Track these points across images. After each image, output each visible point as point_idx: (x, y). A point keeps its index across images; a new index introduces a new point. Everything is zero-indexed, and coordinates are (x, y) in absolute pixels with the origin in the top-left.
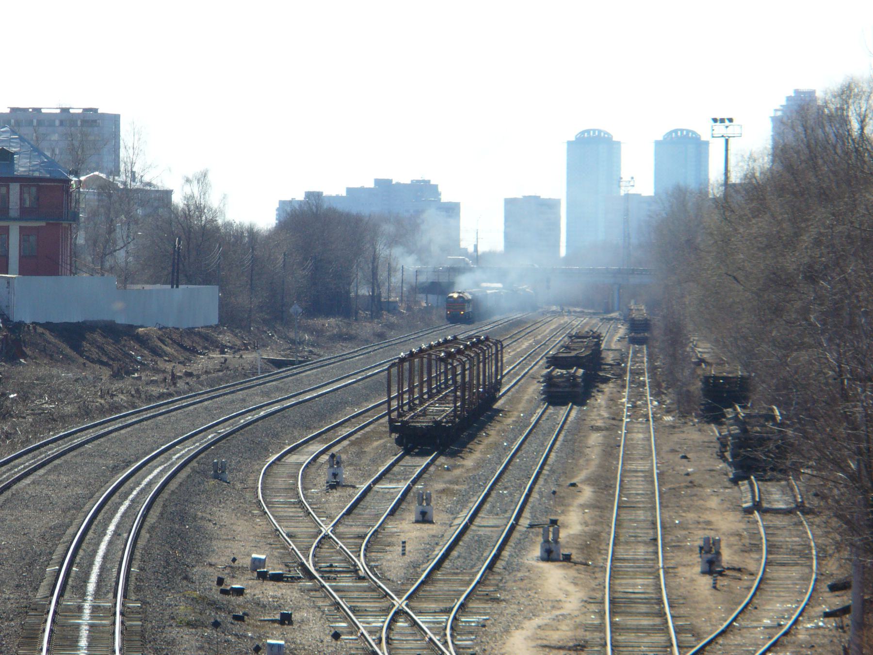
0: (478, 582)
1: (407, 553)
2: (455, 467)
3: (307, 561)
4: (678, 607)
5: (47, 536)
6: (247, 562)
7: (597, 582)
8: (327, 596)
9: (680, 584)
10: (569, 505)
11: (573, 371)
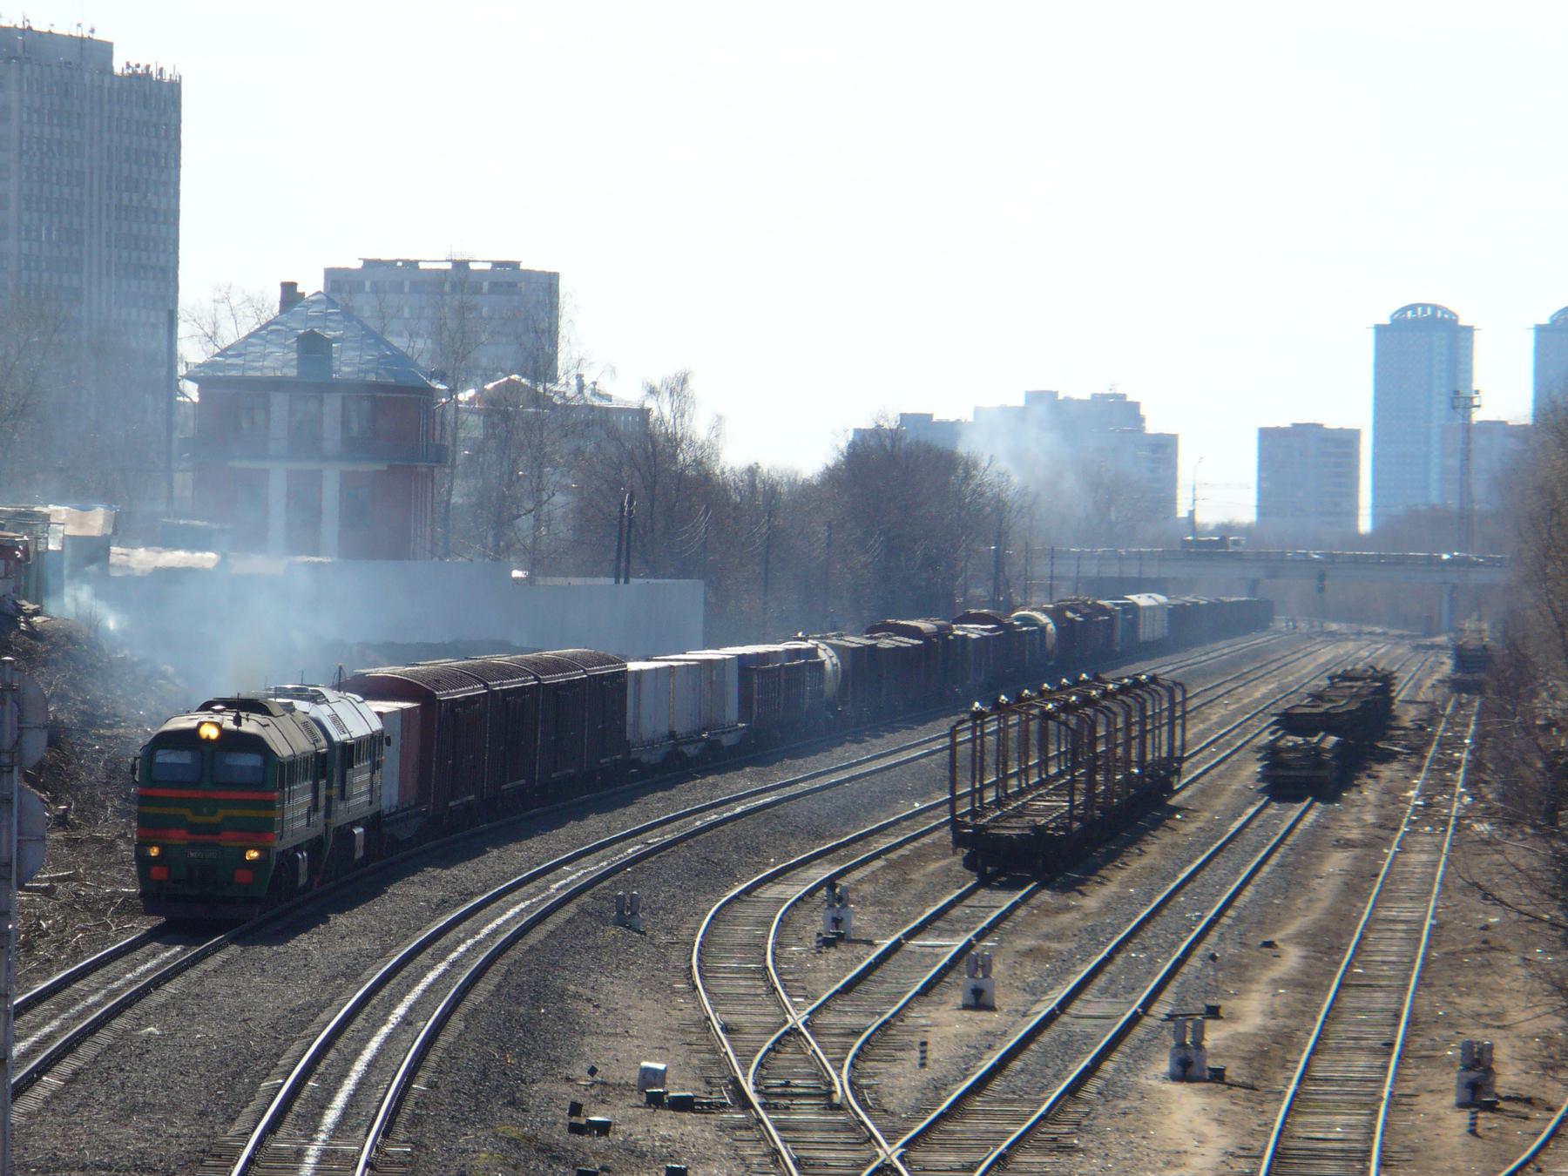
0: (1042, 1117)
1: (929, 1062)
2: (1067, 909)
3: (745, 1075)
4: (1398, 1167)
5: (283, 1024)
6: (633, 1076)
7: (1264, 1118)
8: (765, 1138)
9: (1414, 1125)
10: (1252, 980)
11: (1315, 740)
